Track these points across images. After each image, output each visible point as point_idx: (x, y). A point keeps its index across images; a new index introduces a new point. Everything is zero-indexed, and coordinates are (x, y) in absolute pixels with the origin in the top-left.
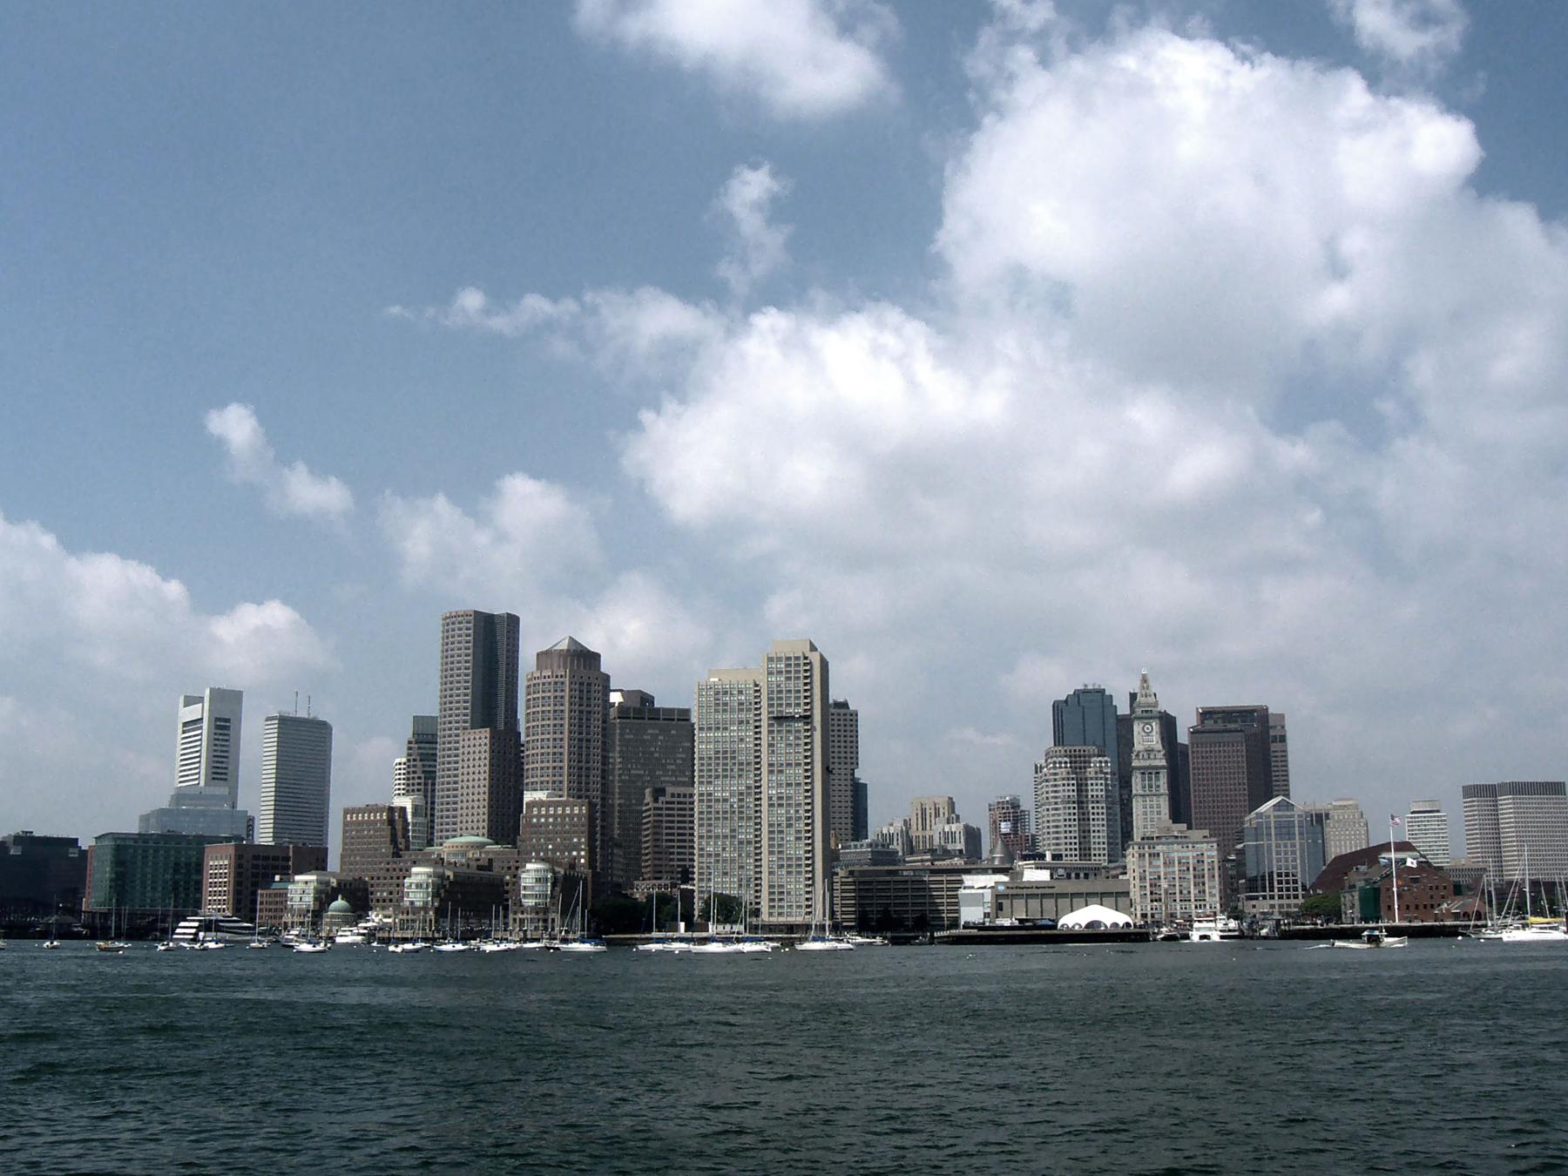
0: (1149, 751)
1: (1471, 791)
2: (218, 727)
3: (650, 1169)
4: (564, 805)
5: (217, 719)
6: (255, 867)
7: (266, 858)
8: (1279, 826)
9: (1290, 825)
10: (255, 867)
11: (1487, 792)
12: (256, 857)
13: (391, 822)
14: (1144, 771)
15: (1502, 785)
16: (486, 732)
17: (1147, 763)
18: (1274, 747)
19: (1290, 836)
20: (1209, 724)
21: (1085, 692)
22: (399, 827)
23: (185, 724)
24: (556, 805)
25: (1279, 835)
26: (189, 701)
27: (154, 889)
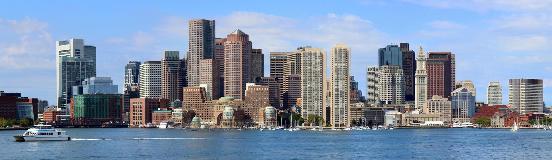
0: (422, 70)
1: (511, 81)
2: (170, 65)
3: (359, 157)
4: (259, 87)
5: (76, 50)
6: (150, 105)
7: (153, 103)
8: (463, 96)
9: (466, 96)
10: (150, 105)
11: (516, 82)
12: (150, 103)
13: (201, 92)
14: (420, 77)
15: (522, 80)
16: (210, 61)
17: (421, 74)
18: (452, 65)
19: (466, 99)
20: (434, 58)
21: (392, 46)
22: (204, 94)
23: (60, 52)
24: (257, 87)
25: (463, 99)
26: (61, 43)
27: (100, 112)
